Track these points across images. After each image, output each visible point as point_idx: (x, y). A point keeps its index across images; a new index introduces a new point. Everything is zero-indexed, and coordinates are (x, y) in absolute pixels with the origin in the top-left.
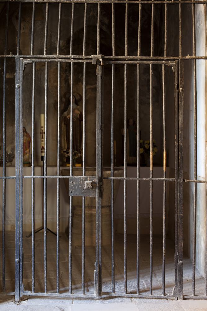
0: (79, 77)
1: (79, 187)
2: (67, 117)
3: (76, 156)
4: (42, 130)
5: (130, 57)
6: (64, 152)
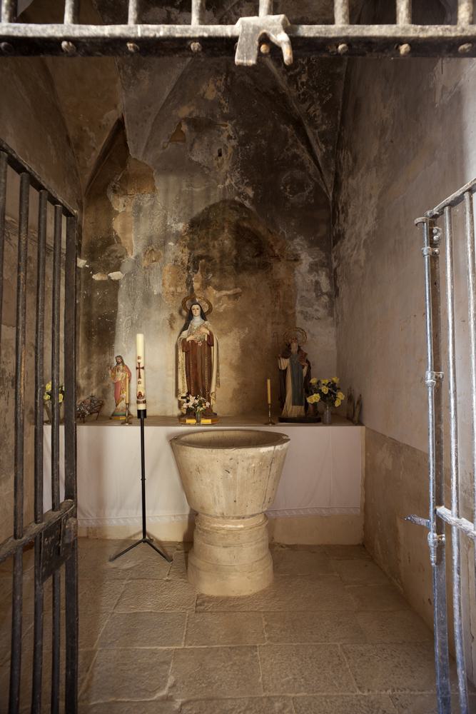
0: (209, 278)
3: (202, 406)
4: (139, 363)
6: (182, 398)
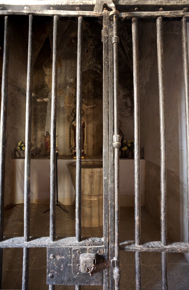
1: (69, 265)
2: (75, 125)
5: (170, 3)
6: (73, 148)
